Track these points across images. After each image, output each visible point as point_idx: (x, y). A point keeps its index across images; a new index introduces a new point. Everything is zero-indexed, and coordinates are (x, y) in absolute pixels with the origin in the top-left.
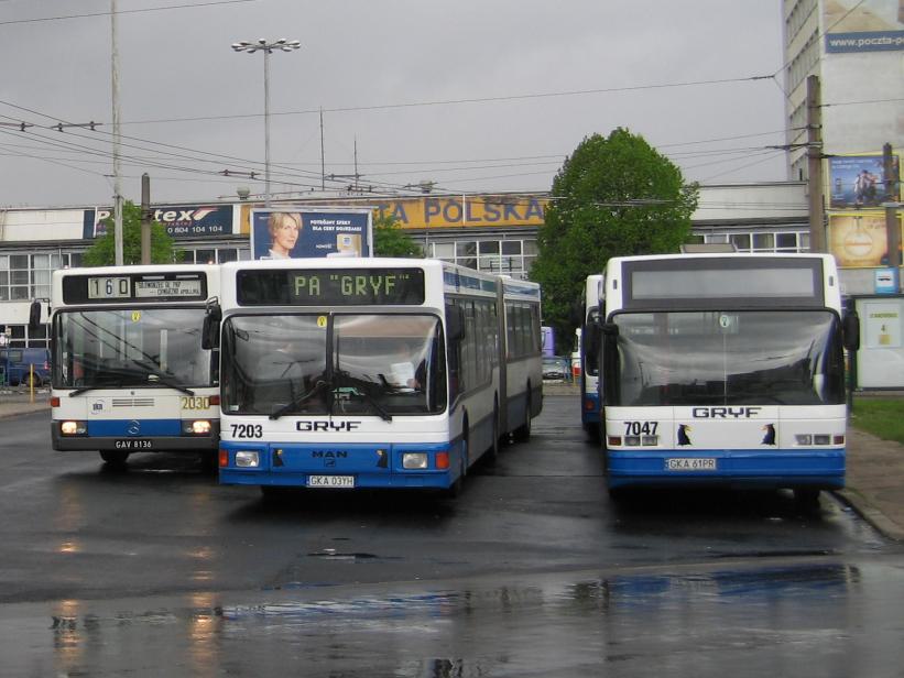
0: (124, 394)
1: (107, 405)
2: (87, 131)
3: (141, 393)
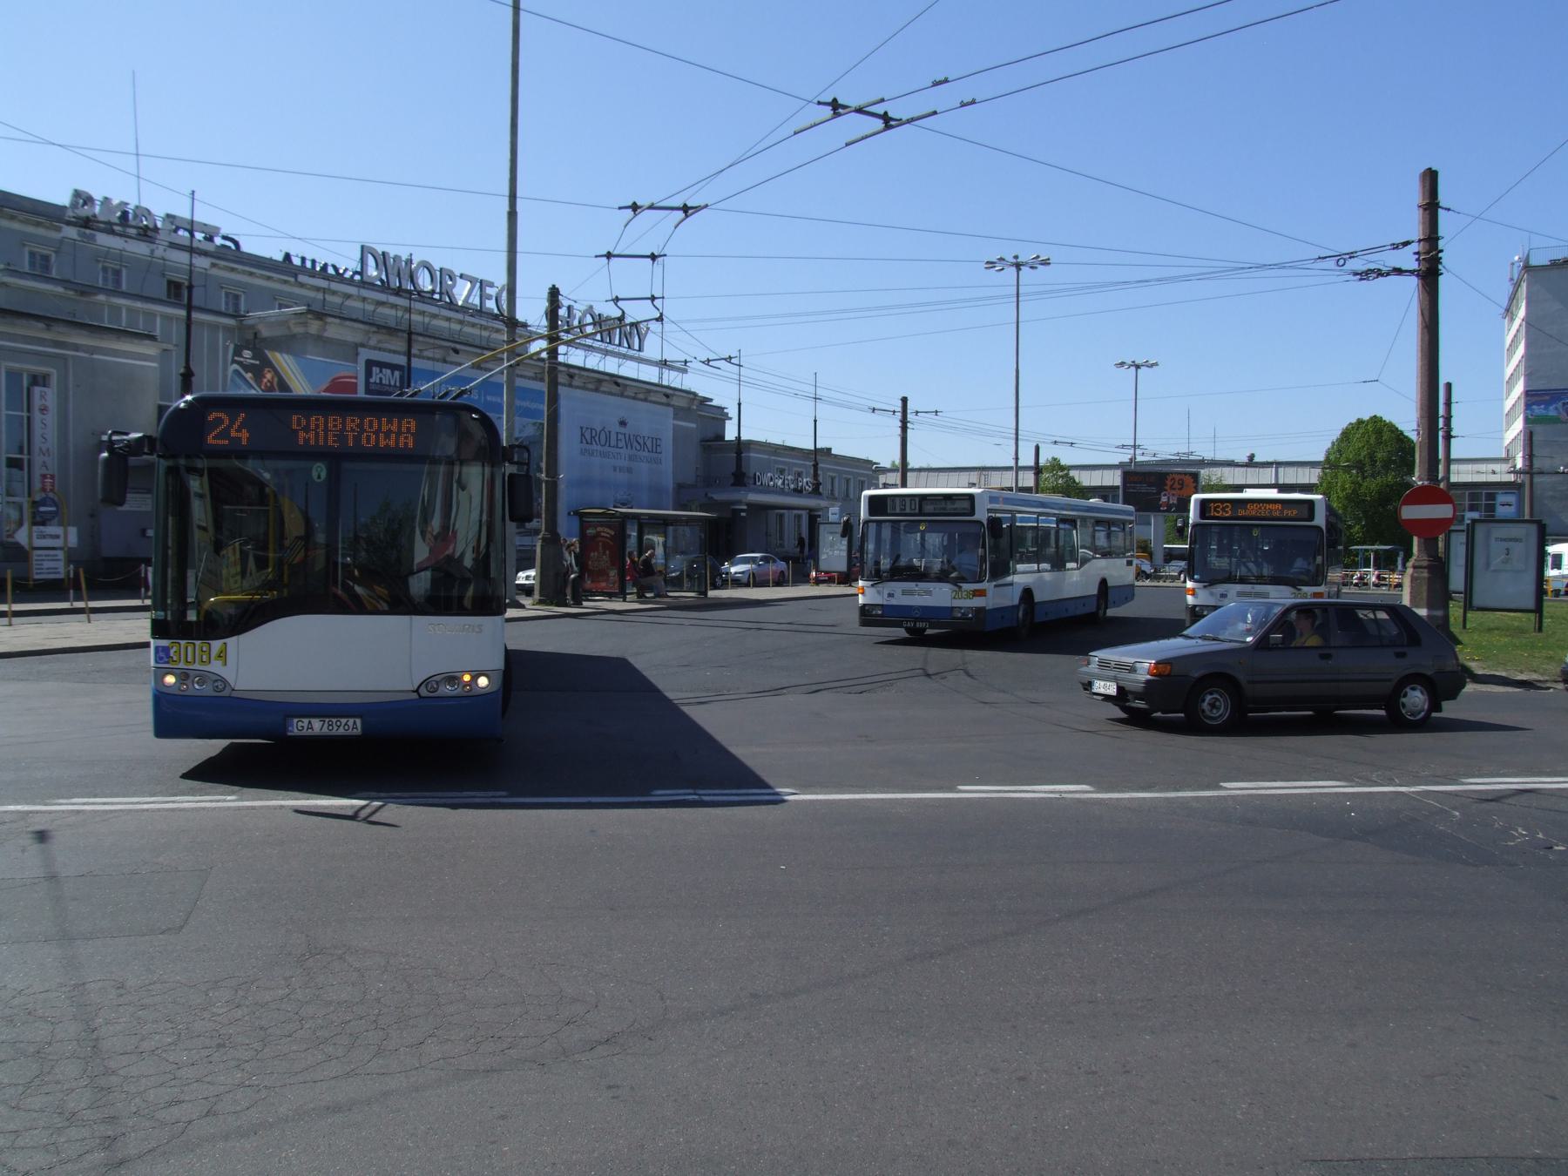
0: (911, 585)
1: (898, 593)
2: (932, 415)
3: (922, 585)
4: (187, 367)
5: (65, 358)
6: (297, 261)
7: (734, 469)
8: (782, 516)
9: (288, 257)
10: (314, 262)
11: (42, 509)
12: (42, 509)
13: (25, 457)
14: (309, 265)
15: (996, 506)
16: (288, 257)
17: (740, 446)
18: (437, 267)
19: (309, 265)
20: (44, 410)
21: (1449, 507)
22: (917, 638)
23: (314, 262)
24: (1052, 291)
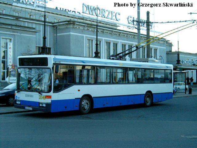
4: (45, 36)
5: (15, 35)
6: (59, 9)
7: (177, 59)
8: (192, 72)
9: (57, 8)
10: (63, 9)
11: (12, 73)
12: (12, 73)
13: (6, 60)
14: (62, 9)
15: (127, 80)
16: (57, 8)
17: (178, 53)
18: (101, 9)
19: (62, 9)
20: (10, 48)
21: (171, 85)
22: (79, 104)
23: (63, 9)
24: (7, 47)
